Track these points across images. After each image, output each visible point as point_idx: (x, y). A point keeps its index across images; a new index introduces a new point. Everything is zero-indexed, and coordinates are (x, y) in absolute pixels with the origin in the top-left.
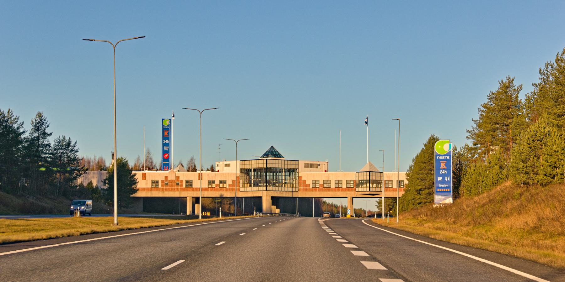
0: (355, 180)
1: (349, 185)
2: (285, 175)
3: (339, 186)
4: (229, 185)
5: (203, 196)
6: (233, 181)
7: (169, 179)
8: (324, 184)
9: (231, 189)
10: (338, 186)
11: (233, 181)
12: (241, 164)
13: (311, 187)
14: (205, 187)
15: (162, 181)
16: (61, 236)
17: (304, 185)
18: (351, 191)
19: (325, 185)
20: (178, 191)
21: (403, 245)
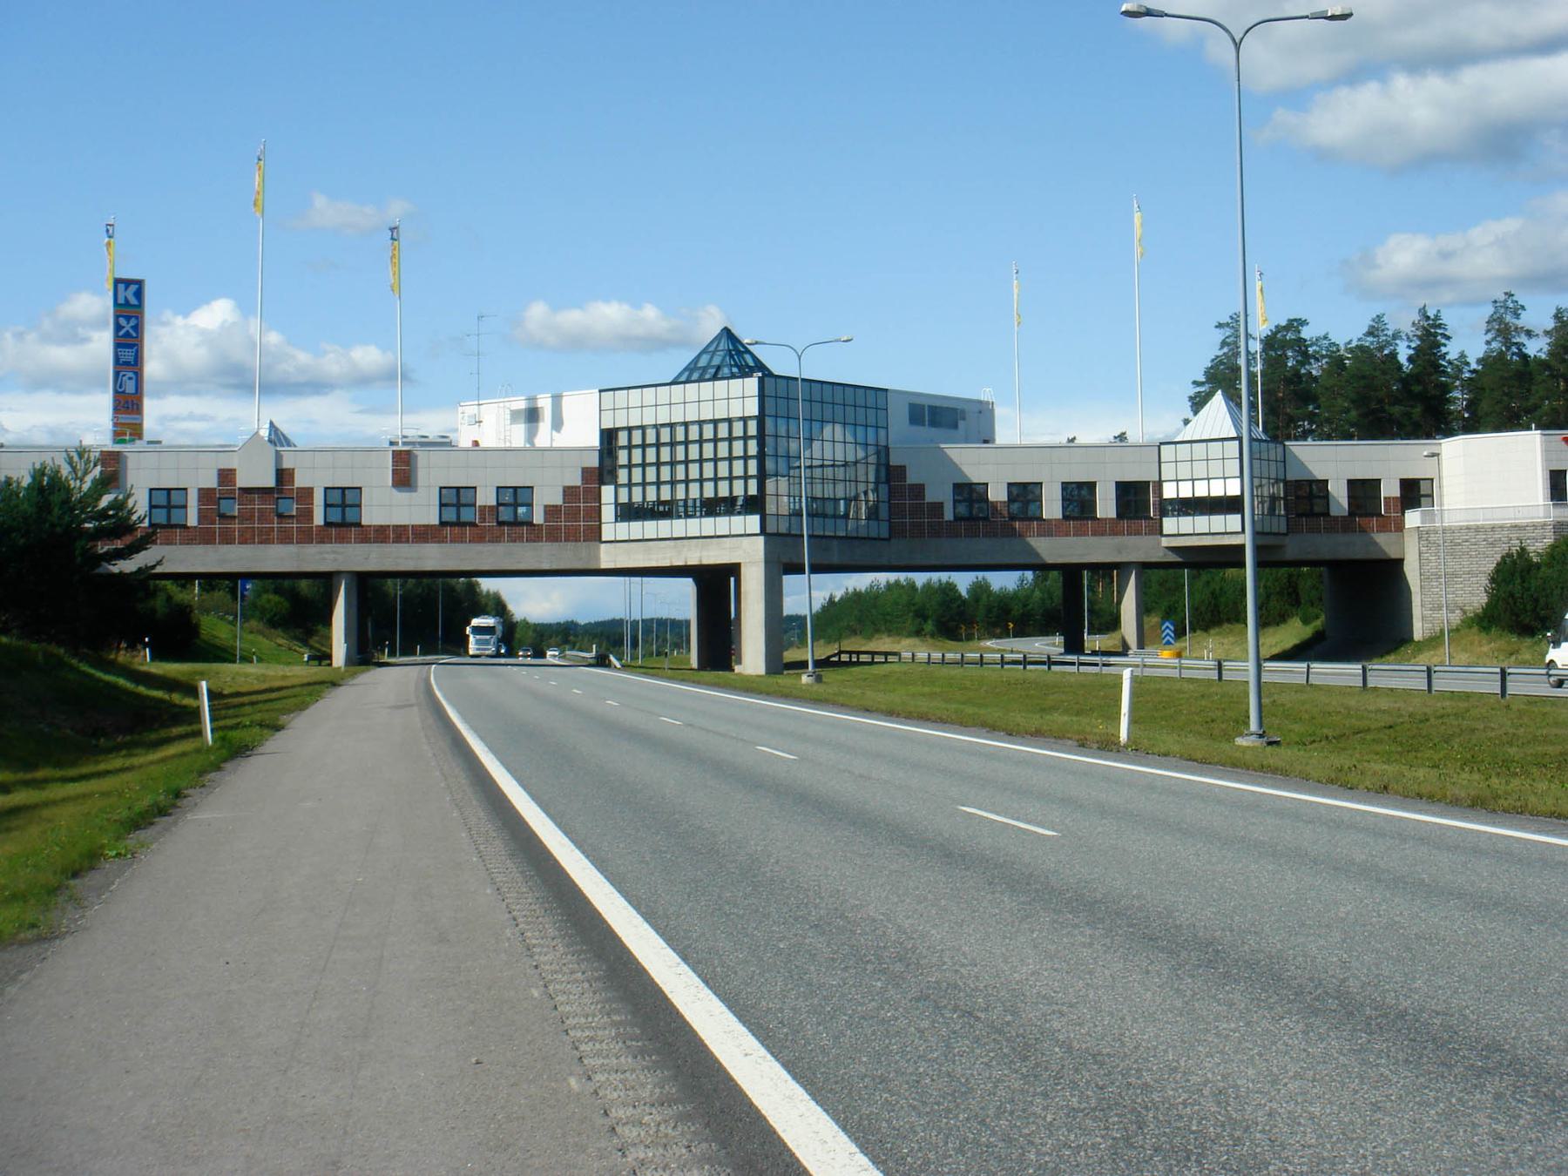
0: (1157, 479)
1: (454, 509)
2: (826, 463)
3: (169, 517)
4: (551, 511)
5: (1260, 530)
6: (569, 492)
7: (242, 481)
8: (499, 504)
9: (558, 528)
10: (163, 521)
11: (569, 492)
12: (882, 432)
13: (322, 523)
14: (425, 522)
15: (205, 495)
16: (222, 765)
17: (573, 514)
18: (1138, 533)
19: (506, 514)
20: (1173, 516)
21: (1360, 1116)
